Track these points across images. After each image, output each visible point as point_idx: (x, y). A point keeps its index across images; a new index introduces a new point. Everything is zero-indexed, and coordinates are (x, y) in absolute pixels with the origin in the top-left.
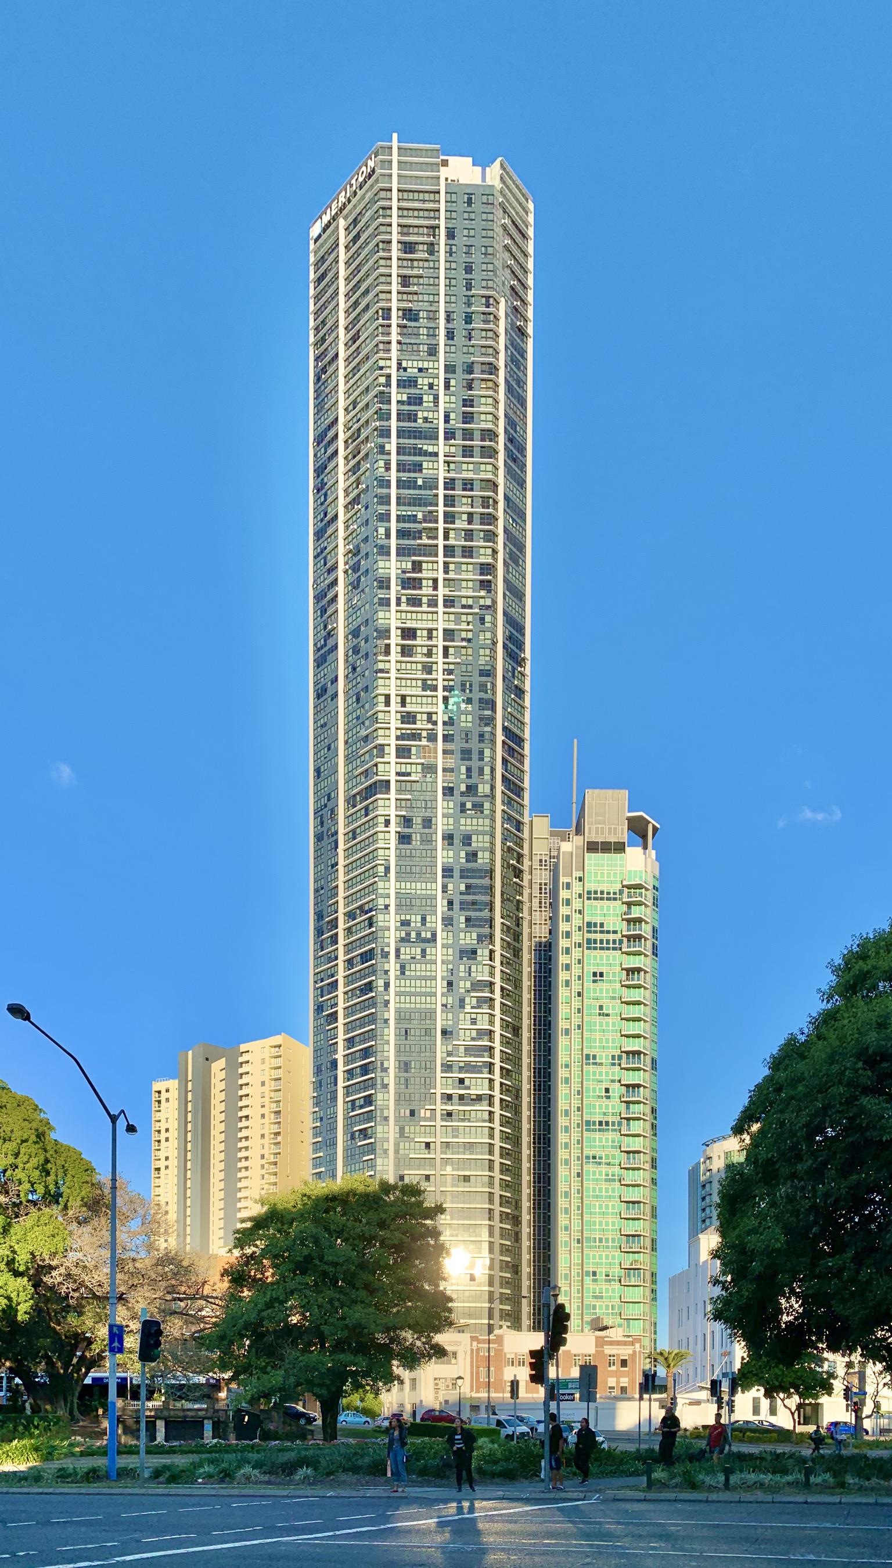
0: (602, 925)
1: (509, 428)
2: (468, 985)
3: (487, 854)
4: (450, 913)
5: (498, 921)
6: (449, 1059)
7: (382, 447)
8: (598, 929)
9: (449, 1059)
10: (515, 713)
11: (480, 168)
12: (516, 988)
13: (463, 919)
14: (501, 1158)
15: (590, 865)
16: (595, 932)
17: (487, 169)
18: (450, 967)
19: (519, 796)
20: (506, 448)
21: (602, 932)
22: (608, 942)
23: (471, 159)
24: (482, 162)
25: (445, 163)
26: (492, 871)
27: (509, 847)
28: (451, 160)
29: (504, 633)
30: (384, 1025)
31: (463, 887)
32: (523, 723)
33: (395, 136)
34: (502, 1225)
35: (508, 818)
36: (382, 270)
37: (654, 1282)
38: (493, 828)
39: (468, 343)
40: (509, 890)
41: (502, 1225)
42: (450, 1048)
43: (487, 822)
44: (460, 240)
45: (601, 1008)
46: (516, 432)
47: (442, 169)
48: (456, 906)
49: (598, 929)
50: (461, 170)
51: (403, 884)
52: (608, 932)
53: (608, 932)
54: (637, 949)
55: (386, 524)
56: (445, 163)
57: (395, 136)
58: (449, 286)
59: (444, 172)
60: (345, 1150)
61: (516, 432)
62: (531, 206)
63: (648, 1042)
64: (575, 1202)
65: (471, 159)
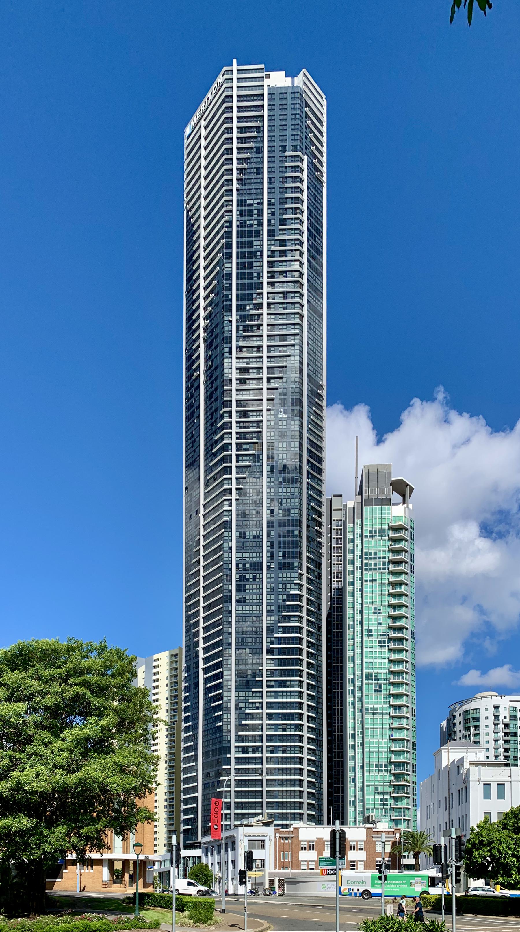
0: (375, 554)
1: (310, 259)
2: (285, 597)
3: (297, 511)
4: (272, 519)
5: (305, 554)
6: (272, 646)
7: (227, 296)
8: (373, 556)
9: (272, 646)
10: (316, 420)
11: (290, 79)
12: (319, 631)
13: (281, 554)
14: (308, 722)
15: (366, 514)
16: (371, 558)
17: (295, 78)
18: (272, 585)
19: (319, 474)
20: (308, 219)
21: (375, 558)
22: (371, 564)
23: (284, 73)
24: (291, 74)
25: (268, 76)
26: (300, 522)
27: (312, 507)
28: (272, 74)
29: (308, 389)
30: (228, 626)
31: (281, 480)
32: (321, 503)
33: (235, 61)
34: (308, 724)
35: (310, 487)
36: (226, 487)
37: (414, 794)
38: (301, 504)
39: (283, 154)
40: (313, 535)
41: (308, 724)
42: (272, 639)
43: (297, 500)
44: (277, 133)
45: (375, 608)
46: (315, 241)
47: (266, 80)
48: (276, 545)
49: (373, 556)
50: (278, 79)
51: (240, 693)
52: (380, 558)
53: (380, 558)
54: (401, 680)
55: (229, 345)
56: (268, 76)
57: (235, 61)
58: (270, 183)
59: (266, 82)
60: (204, 710)
61: (315, 241)
62: (325, 103)
63: (410, 733)
64: (358, 739)
65: (284, 73)
